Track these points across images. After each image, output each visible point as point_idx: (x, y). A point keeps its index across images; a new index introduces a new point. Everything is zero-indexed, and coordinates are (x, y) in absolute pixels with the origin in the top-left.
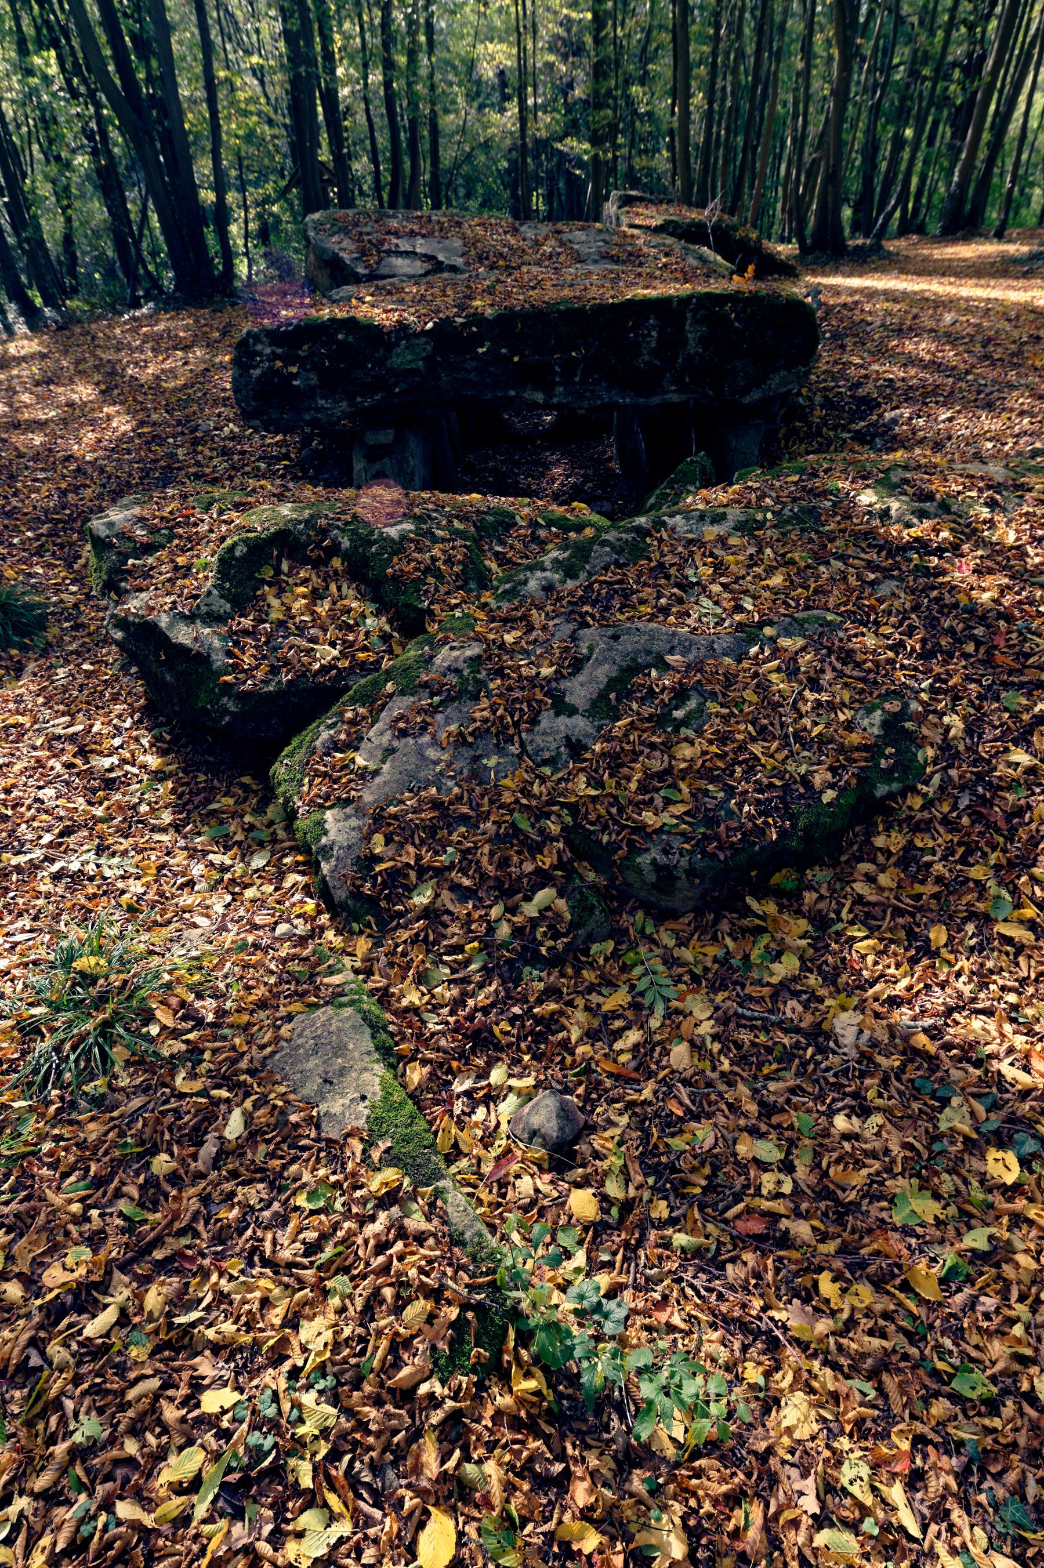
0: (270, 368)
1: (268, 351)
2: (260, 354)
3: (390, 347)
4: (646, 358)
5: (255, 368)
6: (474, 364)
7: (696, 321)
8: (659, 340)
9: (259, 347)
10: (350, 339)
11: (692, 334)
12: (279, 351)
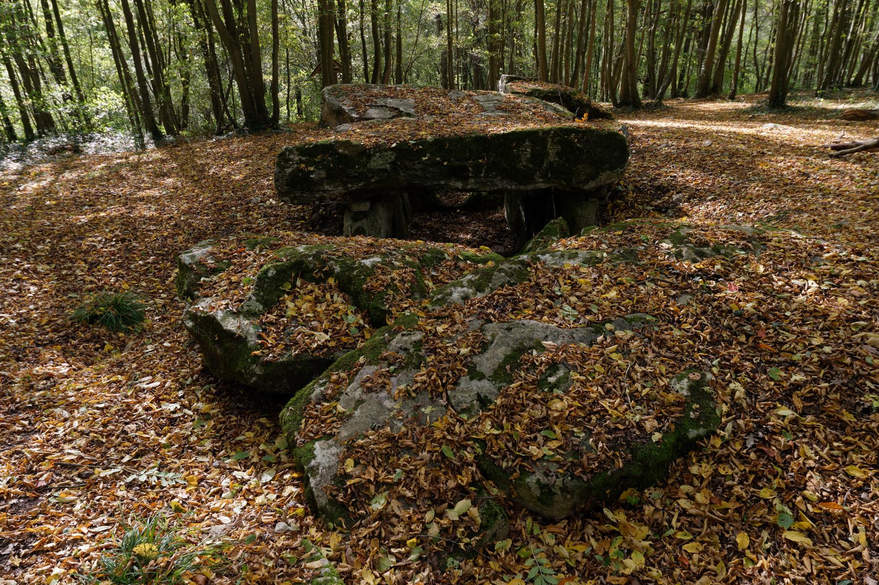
0: (298, 168)
1: (297, 158)
2: (292, 160)
3: (369, 156)
4: (524, 163)
5: (288, 168)
6: (420, 166)
7: (554, 143)
8: (532, 154)
9: (292, 156)
10: (346, 152)
11: (552, 150)
12: (304, 158)
